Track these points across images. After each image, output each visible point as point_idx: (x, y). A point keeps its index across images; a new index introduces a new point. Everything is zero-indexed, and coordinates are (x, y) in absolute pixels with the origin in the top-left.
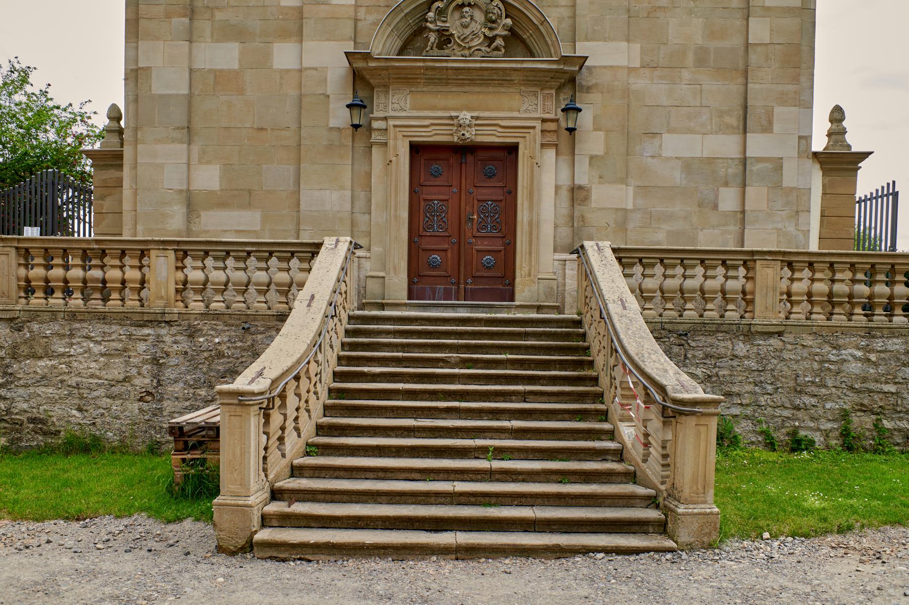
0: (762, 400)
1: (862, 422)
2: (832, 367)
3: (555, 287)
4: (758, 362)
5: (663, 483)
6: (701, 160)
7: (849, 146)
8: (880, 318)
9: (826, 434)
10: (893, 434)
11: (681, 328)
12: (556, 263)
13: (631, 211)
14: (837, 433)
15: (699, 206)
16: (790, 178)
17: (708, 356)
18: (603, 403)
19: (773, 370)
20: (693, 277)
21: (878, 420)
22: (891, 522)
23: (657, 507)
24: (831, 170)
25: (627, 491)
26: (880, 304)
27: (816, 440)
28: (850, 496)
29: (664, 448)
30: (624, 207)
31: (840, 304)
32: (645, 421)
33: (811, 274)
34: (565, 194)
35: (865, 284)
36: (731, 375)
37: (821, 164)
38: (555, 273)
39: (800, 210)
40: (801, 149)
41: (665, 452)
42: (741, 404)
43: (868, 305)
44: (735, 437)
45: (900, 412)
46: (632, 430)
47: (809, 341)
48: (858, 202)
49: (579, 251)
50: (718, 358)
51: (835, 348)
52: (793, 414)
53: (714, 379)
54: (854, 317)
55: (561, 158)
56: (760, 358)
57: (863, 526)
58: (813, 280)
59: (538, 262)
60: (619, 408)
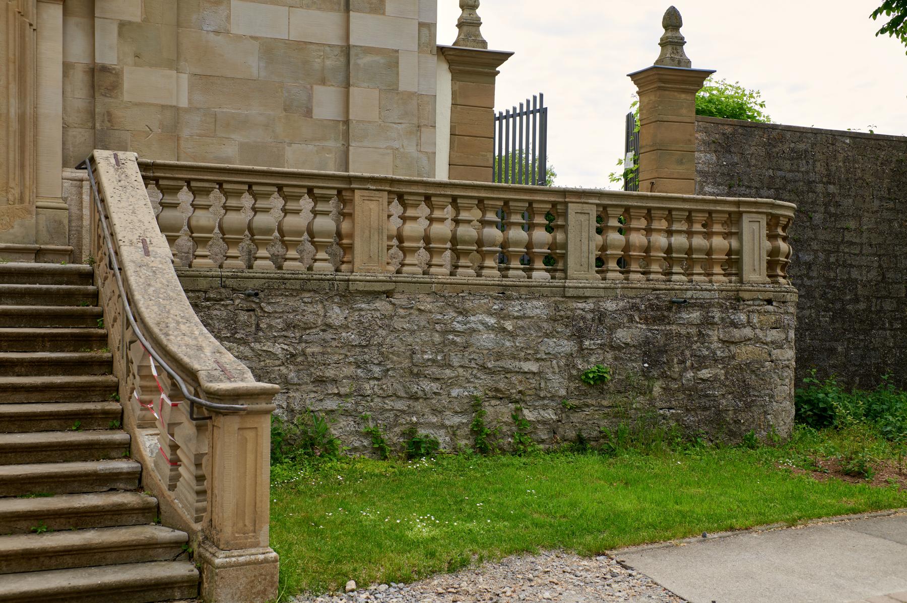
0: (367, 387)
1: (498, 414)
2: (458, 339)
3: (66, 222)
4: (360, 334)
5: (198, 520)
6: (288, 43)
7: (484, 43)
8: (516, 273)
9: (453, 432)
10: (536, 428)
11: (251, 285)
12: (67, 184)
13: (187, 111)
14: (467, 430)
15: (285, 110)
16: (408, 80)
17: (289, 326)
18: (118, 401)
19: (380, 345)
20: (266, 210)
21: (517, 410)
22: (517, 551)
23: (190, 557)
24: (461, 72)
25: (142, 537)
26: (516, 254)
27: (440, 440)
28: (470, 517)
29: (198, 465)
30: (174, 104)
31: (467, 253)
32: (172, 427)
33: (428, 211)
34: (79, 77)
35: (523, 228)
36: (323, 354)
37: (450, 63)
38: (65, 200)
39: (422, 125)
40: (423, 40)
41: (200, 473)
42: (339, 395)
43: (527, 258)
44: (331, 442)
45: (544, 398)
46: (155, 440)
47: (427, 304)
48: (498, 119)
49: (90, 164)
50: (305, 329)
51: (461, 313)
52: (409, 407)
53: (299, 359)
54: (485, 272)
55: (72, 21)
56: (364, 329)
57: (481, 559)
58: (457, 222)
59: (36, 180)
60: (137, 406)
